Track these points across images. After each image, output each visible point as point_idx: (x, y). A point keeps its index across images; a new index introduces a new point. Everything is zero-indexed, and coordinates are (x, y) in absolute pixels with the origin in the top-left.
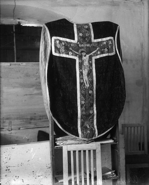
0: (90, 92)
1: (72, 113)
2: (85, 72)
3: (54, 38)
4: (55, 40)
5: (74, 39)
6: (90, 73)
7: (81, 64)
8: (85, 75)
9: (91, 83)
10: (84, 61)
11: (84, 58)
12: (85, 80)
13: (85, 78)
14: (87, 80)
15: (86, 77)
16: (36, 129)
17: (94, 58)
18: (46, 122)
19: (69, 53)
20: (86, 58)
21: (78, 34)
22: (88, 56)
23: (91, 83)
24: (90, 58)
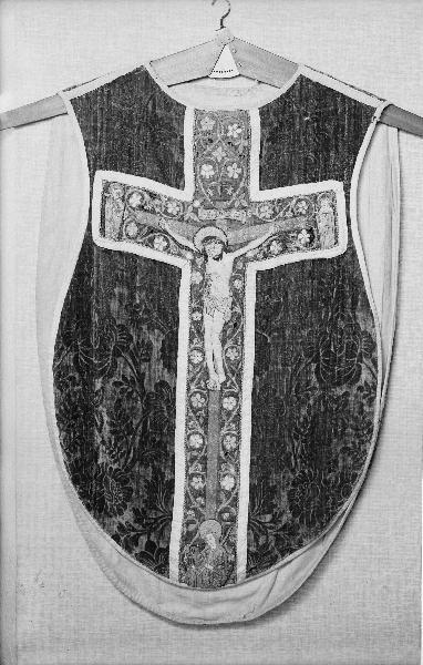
0: (229, 403)
1: (149, 479)
2: (214, 325)
3: (103, 175)
4: (107, 187)
5: (179, 185)
6: (233, 329)
7: (198, 293)
8: (213, 348)
9: (234, 370)
10: (213, 277)
11: (212, 266)
12: (209, 355)
13: (212, 342)
14: (218, 355)
15: (217, 346)
16: (41, 123)
17: (252, 270)
18: (49, 445)
19: (156, 240)
20: (221, 270)
21: (238, 407)
22: (228, 258)
23: (234, 370)
24: (238, 273)
